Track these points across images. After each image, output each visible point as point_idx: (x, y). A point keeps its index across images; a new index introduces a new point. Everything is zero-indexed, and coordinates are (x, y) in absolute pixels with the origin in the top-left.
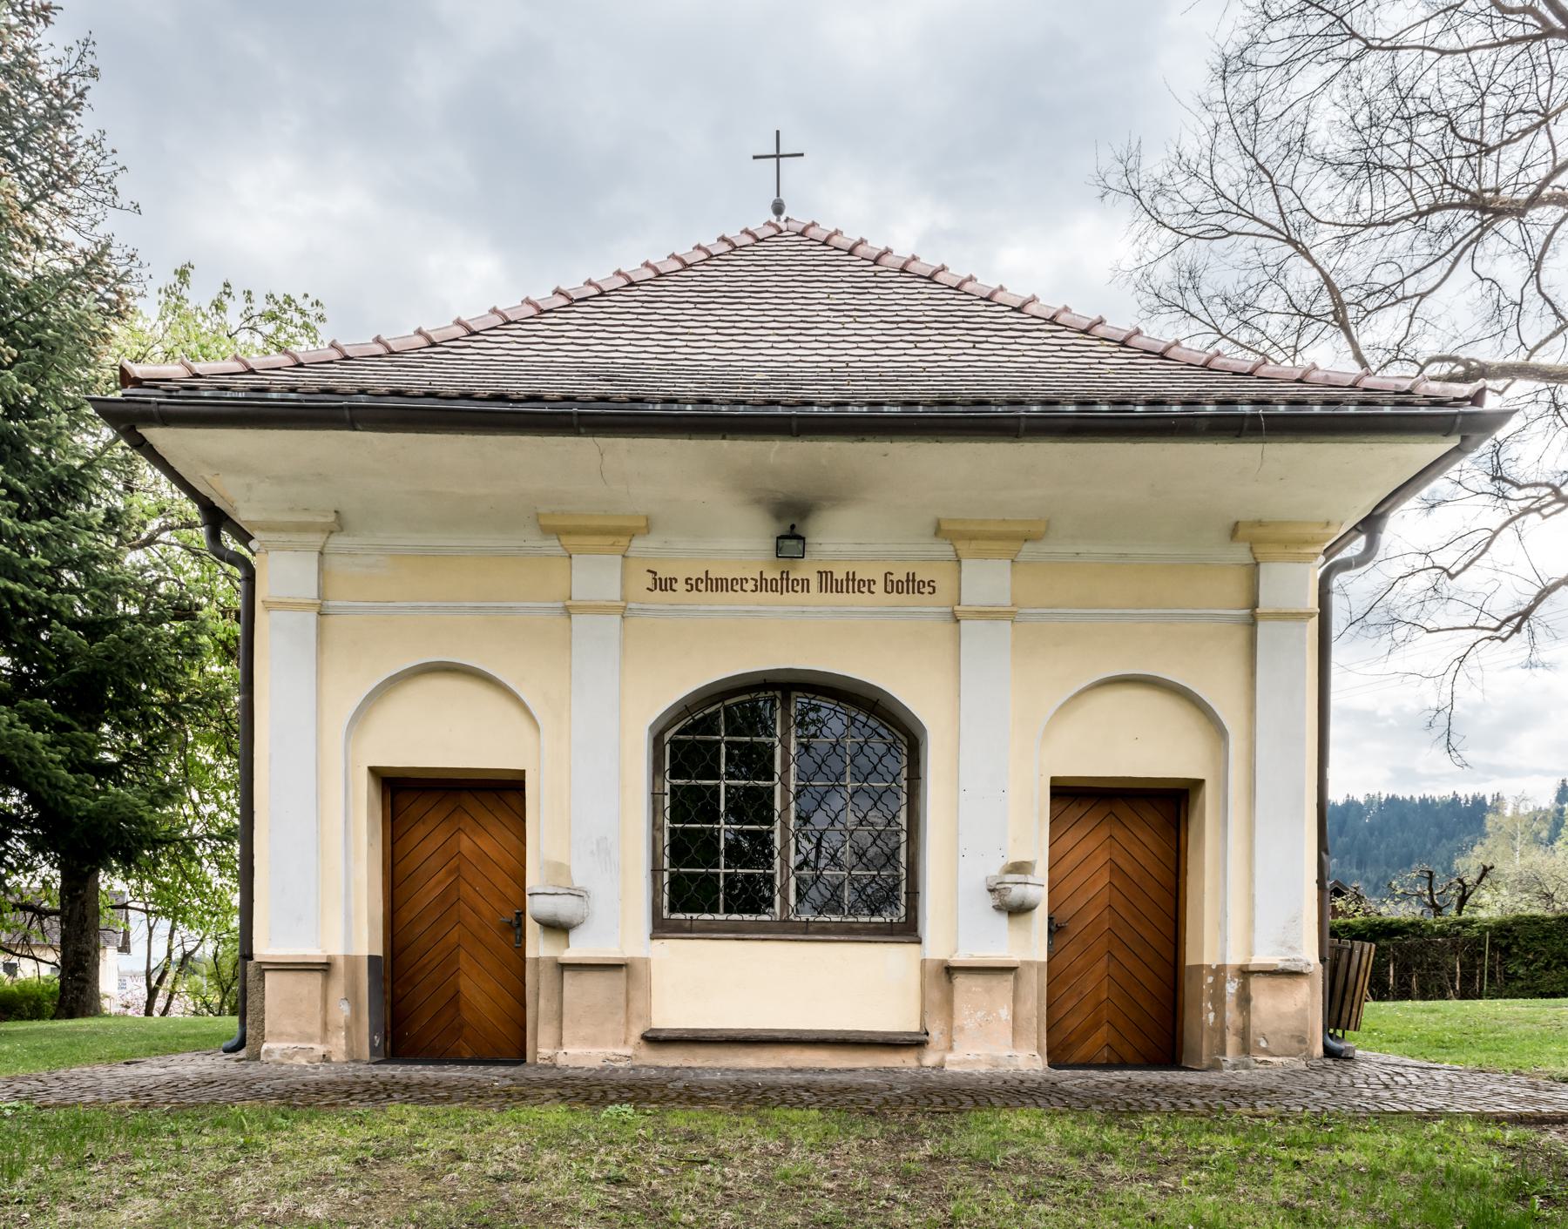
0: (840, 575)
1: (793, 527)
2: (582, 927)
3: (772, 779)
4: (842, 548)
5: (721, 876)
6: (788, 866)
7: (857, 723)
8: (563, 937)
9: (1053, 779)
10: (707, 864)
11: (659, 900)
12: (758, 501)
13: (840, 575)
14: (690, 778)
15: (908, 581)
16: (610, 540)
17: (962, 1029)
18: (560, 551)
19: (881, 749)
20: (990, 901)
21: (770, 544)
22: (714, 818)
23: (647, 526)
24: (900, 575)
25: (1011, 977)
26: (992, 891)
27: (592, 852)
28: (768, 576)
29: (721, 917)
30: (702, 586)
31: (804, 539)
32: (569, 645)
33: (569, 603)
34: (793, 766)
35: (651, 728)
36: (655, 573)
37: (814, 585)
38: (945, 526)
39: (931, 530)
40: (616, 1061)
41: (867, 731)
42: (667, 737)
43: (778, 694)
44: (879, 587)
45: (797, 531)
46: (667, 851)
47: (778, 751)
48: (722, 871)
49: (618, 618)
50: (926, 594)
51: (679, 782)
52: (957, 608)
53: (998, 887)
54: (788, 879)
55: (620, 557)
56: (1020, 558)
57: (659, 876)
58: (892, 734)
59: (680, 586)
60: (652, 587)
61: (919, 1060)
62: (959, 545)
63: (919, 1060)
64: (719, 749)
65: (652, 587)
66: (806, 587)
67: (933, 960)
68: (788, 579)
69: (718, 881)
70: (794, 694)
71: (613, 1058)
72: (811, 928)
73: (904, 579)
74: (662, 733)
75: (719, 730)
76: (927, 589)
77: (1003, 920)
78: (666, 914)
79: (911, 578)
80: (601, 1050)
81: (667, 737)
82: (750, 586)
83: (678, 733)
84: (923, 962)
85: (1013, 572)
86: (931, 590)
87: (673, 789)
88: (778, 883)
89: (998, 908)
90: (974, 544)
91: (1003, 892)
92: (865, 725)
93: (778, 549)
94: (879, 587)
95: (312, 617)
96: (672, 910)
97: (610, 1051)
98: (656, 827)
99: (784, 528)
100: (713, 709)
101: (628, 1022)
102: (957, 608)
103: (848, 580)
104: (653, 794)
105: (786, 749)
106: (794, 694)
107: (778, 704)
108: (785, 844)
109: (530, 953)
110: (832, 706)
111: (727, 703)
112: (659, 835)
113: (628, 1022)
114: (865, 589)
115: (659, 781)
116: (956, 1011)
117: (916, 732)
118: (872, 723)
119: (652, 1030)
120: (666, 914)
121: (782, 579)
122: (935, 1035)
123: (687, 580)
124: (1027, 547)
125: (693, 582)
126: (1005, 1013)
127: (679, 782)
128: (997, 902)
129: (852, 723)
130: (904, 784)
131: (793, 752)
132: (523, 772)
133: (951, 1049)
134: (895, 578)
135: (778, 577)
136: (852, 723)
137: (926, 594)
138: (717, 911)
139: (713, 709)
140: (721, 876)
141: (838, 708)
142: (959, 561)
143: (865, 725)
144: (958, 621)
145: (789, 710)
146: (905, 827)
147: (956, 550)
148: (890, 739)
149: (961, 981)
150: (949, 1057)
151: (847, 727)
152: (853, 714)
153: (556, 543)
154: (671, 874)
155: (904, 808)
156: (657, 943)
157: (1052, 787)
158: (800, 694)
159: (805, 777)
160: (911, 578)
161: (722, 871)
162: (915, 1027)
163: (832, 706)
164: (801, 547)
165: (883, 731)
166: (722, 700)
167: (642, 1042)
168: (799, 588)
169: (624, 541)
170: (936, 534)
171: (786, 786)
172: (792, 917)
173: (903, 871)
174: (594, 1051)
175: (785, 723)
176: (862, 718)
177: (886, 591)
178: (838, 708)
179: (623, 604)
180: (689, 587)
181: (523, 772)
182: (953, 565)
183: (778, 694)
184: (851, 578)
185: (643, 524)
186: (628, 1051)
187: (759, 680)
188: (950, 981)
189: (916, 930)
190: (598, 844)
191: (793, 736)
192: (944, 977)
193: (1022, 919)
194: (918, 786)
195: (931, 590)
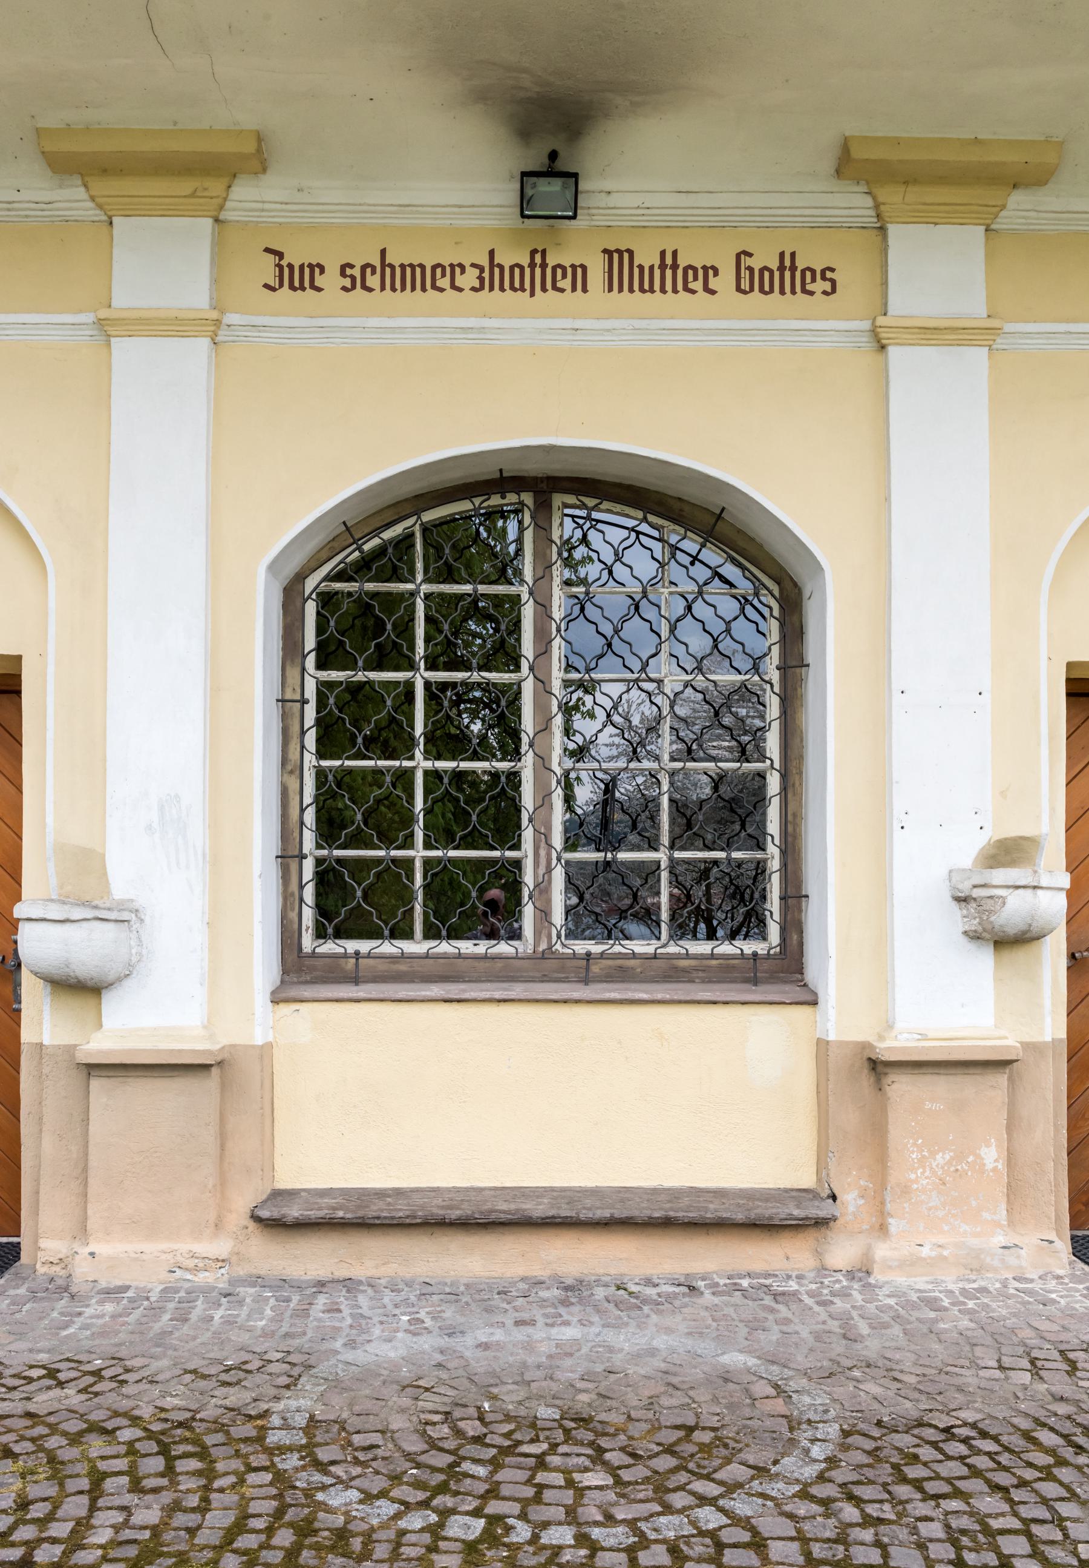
0: (647, 257)
1: (553, 156)
2: (127, 983)
3: (518, 668)
4: (650, 200)
5: (418, 864)
6: (550, 846)
7: (679, 555)
8: (91, 1001)
9: (1070, 666)
10: (388, 841)
11: (294, 915)
12: (481, 96)
13: (647, 257)
14: (353, 666)
15: (782, 268)
16: (186, 186)
17: (905, 1190)
18: (87, 210)
19: (729, 607)
20: (956, 920)
21: (510, 193)
22: (407, 748)
23: (259, 150)
24: (765, 257)
25: (1002, 1079)
26: (962, 900)
27: (149, 828)
28: (505, 259)
29: (416, 947)
30: (373, 281)
31: (575, 176)
32: (103, 399)
33: (103, 313)
34: (557, 642)
35: (273, 567)
36: (280, 255)
37: (596, 276)
38: (857, 153)
39: (828, 165)
40: (196, 1269)
41: (701, 573)
42: (310, 584)
43: (528, 498)
44: (724, 282)
45: (561, 165)
46: (310, 817)
47: (528, 613)
48: (419, 853)
49: (204, 343)
50: (818, 295)
51: (335, 675)
52: (881, 321)
53: (977, 893)
54: (549, 870)
55: (210, 221)
56: (1002, 223)
57: (294, 865)
58: (753, 579)
59: (332, 280)
60: (273, 282)
61: (818, 1254)
62: (885, 194)
63: (818, 1254)
64: (411, 610)
65: (273, 282)
66: (579, 276)
67: (842, 1044)
68: (544, 266)
69: (411, 877)
70: (558, 499)
71: (191, 1263)
72: (595, 969)
73: (774, 265)
74: (300, 577)
75: (412, 571)
76: (820, 286)
77: (984, 958)
78: (308, 942)
79: (787, 264)
80: (165, 1246)
81: (310, 584)
82: (469, 279)
83: (329, 578)
84: (822, 1046)
85: (990, 256)
86: (827, 286)
87: (324, 689)
88: (528, 878)
89: (974, 937)
90: (914, 194)
91: (988, 905)
92: (695, 559)
93: (525, 205)
94: (724, 282)
95: (694, 554)
96: (320, 934)
97: (185, 1246)
98: (289, 767)
99: (536, 160)
100: (396, 531)
101: (223, 1181)
102: (881, 321)
103: (663, 266)
104: (282, 700)
105: (543, 607)
106: (558, 499)
107: (527, 520)
108: (544, 800)
109: (27, 1036)
110: (631, 523)
111: (429, 516)
112: (293, 784)
113: (223, 1181)
114: (698, 285)
115: (294, 674)
116: (892, 1153)
117: (798, 571)
118: (712, 556)
119: (277, 1195)
120: (308, 942)
121: (532, 265)
122: (851, 1200)
123: (343, 268)
124: (1018, 199)
125: (356, 272)
126: (991, 1156)
127: (335, 675)
128: (974, 925)
129: (673, 556)
130: (775, 676)
131: (557, 614)
132: (19, 658)
133: (883, 1229)
134: (756, 263)
135: (525, 261)
136: (673, 556)
137: (818, 295)
138: (408, 935)
139: (396, 531)
140: (418, 864)
141: (644, 528)
142: (882, 230)
143: (695, 559)
144: (883, 347)
145: (548, 530)
146: (777, 765)
147: (877, 206)
148: (744, 586)
149: (900, 1086)
150: (882, 1251)
151: (662, 565)
152: (673, 539)
153: (81, 193)
154: (319, 862)
155: (776, 726)
156: (286, 1009)
157: (1069, 681)
158: (571, 499)
159: (580, 664)
160: (787, 264)
161: (419, 853)
162: (806, 1179)
163: (631, 523)
164: (569, 195)
165: (730, 571)
166: (417, 513)
167: (252, 1225)
168: (566, 284)
169: (215, 186)
170: (838, 173)
171: (543, 684)
172: (558, 947)
173: (773, 850)
174: (152, 1248)
175: (540, 556)
176: (691, 545)
177: (739, 289)
178: (644, 528)
179: (214, 315)
180: (347, 283)
181: (19, 658)
182: (874, 237)
183: (528, 498)
184: (669, 262)
185: (250, 147)
186: (222, 1247)
187: (488, 472)
188: (878, 1080)
189: (800, 970)
190: (161, 808)
191: (557, 581)
192: (866, 1080)
193: (1020, 955)
194: (801, 681)
195: (827, 286)
